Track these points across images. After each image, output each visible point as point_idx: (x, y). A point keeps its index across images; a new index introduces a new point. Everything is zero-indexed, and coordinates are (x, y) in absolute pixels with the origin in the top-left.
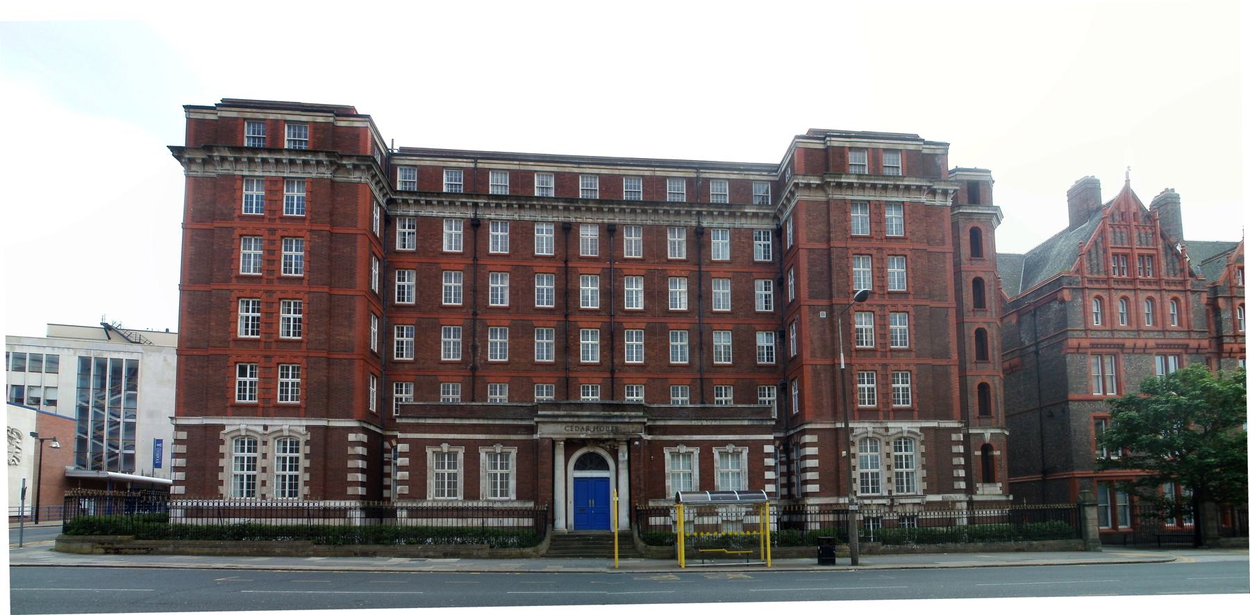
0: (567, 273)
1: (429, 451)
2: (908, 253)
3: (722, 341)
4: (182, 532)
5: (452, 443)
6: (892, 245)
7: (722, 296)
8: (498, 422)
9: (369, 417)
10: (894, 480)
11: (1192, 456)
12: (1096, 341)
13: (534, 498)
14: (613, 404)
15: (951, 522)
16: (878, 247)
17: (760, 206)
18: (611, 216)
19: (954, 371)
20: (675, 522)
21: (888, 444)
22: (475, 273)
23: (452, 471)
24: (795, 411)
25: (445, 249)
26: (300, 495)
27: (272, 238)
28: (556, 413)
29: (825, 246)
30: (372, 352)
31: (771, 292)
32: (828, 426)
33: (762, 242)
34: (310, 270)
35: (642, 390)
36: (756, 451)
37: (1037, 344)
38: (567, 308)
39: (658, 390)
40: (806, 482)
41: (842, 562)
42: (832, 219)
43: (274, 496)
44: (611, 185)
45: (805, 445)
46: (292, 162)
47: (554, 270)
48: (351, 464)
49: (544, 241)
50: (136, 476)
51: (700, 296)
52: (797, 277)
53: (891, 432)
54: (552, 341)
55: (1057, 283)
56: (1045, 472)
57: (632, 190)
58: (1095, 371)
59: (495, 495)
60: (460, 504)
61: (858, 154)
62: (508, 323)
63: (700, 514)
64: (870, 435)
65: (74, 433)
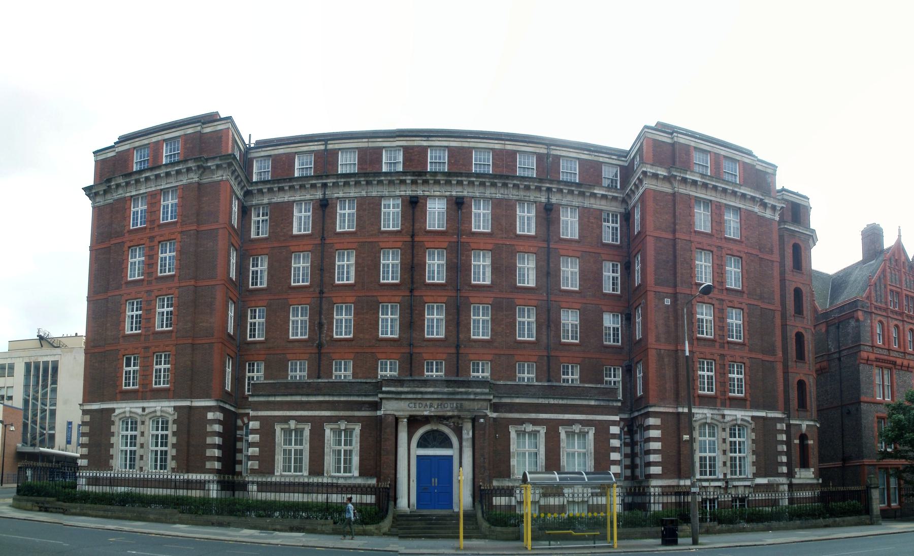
0: (413, 247)
1: (278, 428)
2: (743, 255)
3: (570, 319)
4: (86, 498)
5: (299, 419)
6: (731, 246)
7: (570, 274)
9: (225, 397)
10: (728, 464)
12: (879, 356)
13: (377, 475)
14: (457, 379)
15: (775, 503)
17: (609, 188)
18: (459, 189)
19: (779, 367)
21: (724, 430)
22: (322, 252)
23: (298, 447)
24: (640, 393)
25: (295, 232)
26: (169, 468)
28: (400, 389)
29: (671, 237)
30: (229, 335)
31: (619, 275)
32: (671, 410)
33: (610, 224)
36: (602, 431)
37: (840, 352)
38: (413, 282)
39: (505, 364)
40: (649, 464)
42: (678, 211)
43: (149, 470)
44: (460, 157)
45: (649, 428)
50: (55, 451)
51: (548, 274)
52: (644, 262)
53: (728, 419)
54: (397, 317)
55: (854, 305)
56: (844, 460)
58: (878, 380)
59: (339, 471)
60: (306, 480)
63: (545, 495)
64: (709, 421)
65: (21, 420)
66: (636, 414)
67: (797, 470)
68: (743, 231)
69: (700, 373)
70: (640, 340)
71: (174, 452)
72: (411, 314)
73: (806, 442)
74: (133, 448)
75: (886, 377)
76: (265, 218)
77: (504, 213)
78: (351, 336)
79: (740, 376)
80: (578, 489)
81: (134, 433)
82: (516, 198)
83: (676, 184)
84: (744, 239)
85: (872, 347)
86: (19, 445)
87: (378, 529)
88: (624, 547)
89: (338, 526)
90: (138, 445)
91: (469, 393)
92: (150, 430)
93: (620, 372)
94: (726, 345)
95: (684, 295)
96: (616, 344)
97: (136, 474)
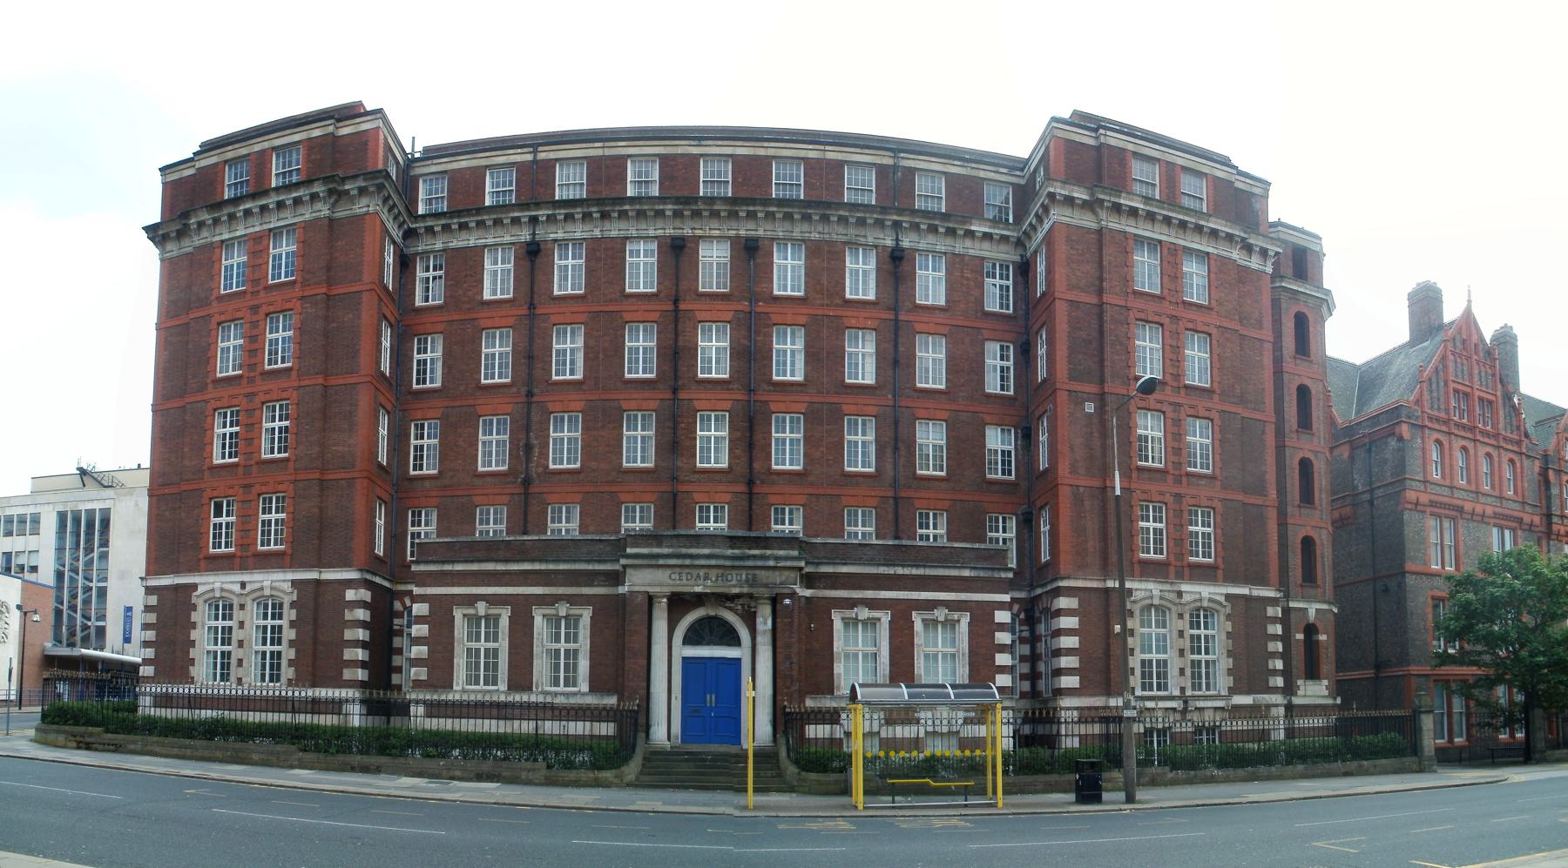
1: (458, 614)
2: (1214, 331)
3: (931, 437)
5: (493, 600)
6: (1191, 314)
7: (931, 363)
8: (562, 567)
9: (374, 564)
10: (1188, 672)
11: (1524, 653)
12: (1435, 498)
13: (617, 688)
14: (750, 535)
15: (1263, 735)
16: (1173, 316)
18: (751, 225)
19: (1272, 514)
20: (848, 734)
21: (1181, 616)
22: (531, 329)
23: (491, 645)
24: (1045, 557)
25: (487, 296)
26: (283, 679)
27: (255, 318)
29: (1095, 301)
30: (380, 465)
31: (1011, 363)
32: (1094, 584)
33: (998, 281)
34: (300, 357)
35: (799, 515)
37: (1371, 491)
38: (676, 378)
40: (1059, 672)
41: (1112, 797)
42: (1106, 259)
43: (251, 681)
44: (751, 173)
45: (1059, 613)
46: (280, 205)
47: (656, 316)
48: (349, 634)
49: (642, 270)
51: (896, 363)
52: (1051, 342)
53: (1186, 598)
54: (652, 433)
55: (1395, 412)
56: (1378, 667)
57: (787, 181)
58: (1433, 538)
59: (557, 684)
60: (503, 698)
61: (1146, 166)
62: (581, 405)
63: (889, 722)
64: (1156, 601)
65: (52, 604)
66: (1039, 591)
67: (1300, 682)
69: (1142, 524)
70: (1046, 470)
71: (292, 654)
72: (675, 428)
78: (578, 465)
81: (227, 623)
82: (844, 239)
86: (49, 645)
88: (1014, 806)
92: (252, 617)
93: (1013, 524)
94: (1184, 479)
96: (1006, 477)
97: (230, 689)
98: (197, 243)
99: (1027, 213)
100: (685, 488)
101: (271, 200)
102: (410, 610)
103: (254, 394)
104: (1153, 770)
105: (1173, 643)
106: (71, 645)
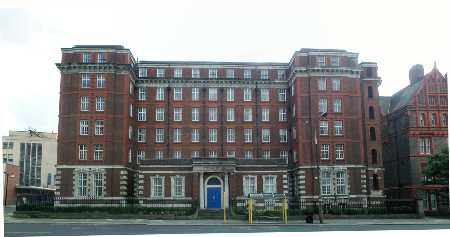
0: (204, 107)
1: (151, 178)
2: (342, 97)
3: (266, 133)
5: (160, 174)
6: (336, 94)
7: (266, 115)
8: (178, 166)
9: (128, 165)
10: (336, 189)
13: (192, 196)
14: (222, 158)
17: (281, 79)
18: (222, 84)
21: (334, 174)
22: (169, 108)
23: (160, 186)
24: (295, 161)
25: (157, 99)
26: (103, 195)
27: (93, 97)
28: (200, 162)
30: (130, 139)
32: (309, 167)
33: (282, 94)
34: (107, 109)
35: (234, 153)
37: (396, 133)
38: (204, 121)
41: (316, 222)
43: (93, 196)
45: (300, 175)
46: (100, 68)
48: (121, 183)
49: (195, 95)
50: (41, 188)
51: (257, 116)
52: (296, 107)
53: (336, 169)
54: (199, 134)
55: (405, 108)
56: (400, 186)
58: (421, 144)
59: (177, 195)
60: (163, 199)
61: (321, 58)
63: (257, 202)
64: (327, 171)
65: (19, 172)
66: (294, 169)
67: (372, 191)
68: (342, 86)
69: (322, 150)
70: (295, 139)
71: (105, 188)
72: (204, 133)
73: (377, 178)
74: (85, 186)
75: (427, 142)
76: (145, 92)
77: (239, 93)
78: (181, 142)
79: (341, 150)
80: (270, 200)
81: (85, 179)
83: (310, 73)
84: (342, 90)
85: (417, 128)
86: (18, 185)
87: (193, 217)
88: (290, 223)
89: (177, 216)
90: (87, 185)
91: (227, 163)
92: (93, 178)
93: (287, 153)
94: (334, 138)
95: (314, 117)
97: (86, 198)
98: (74, 72)
99: (289, 76)
100: (207, 147)
101: (97, 66)
102: (138, 177)
103: (93, 117)
104: (327, 215)
105: (332, 181)
106: (27, 185)
